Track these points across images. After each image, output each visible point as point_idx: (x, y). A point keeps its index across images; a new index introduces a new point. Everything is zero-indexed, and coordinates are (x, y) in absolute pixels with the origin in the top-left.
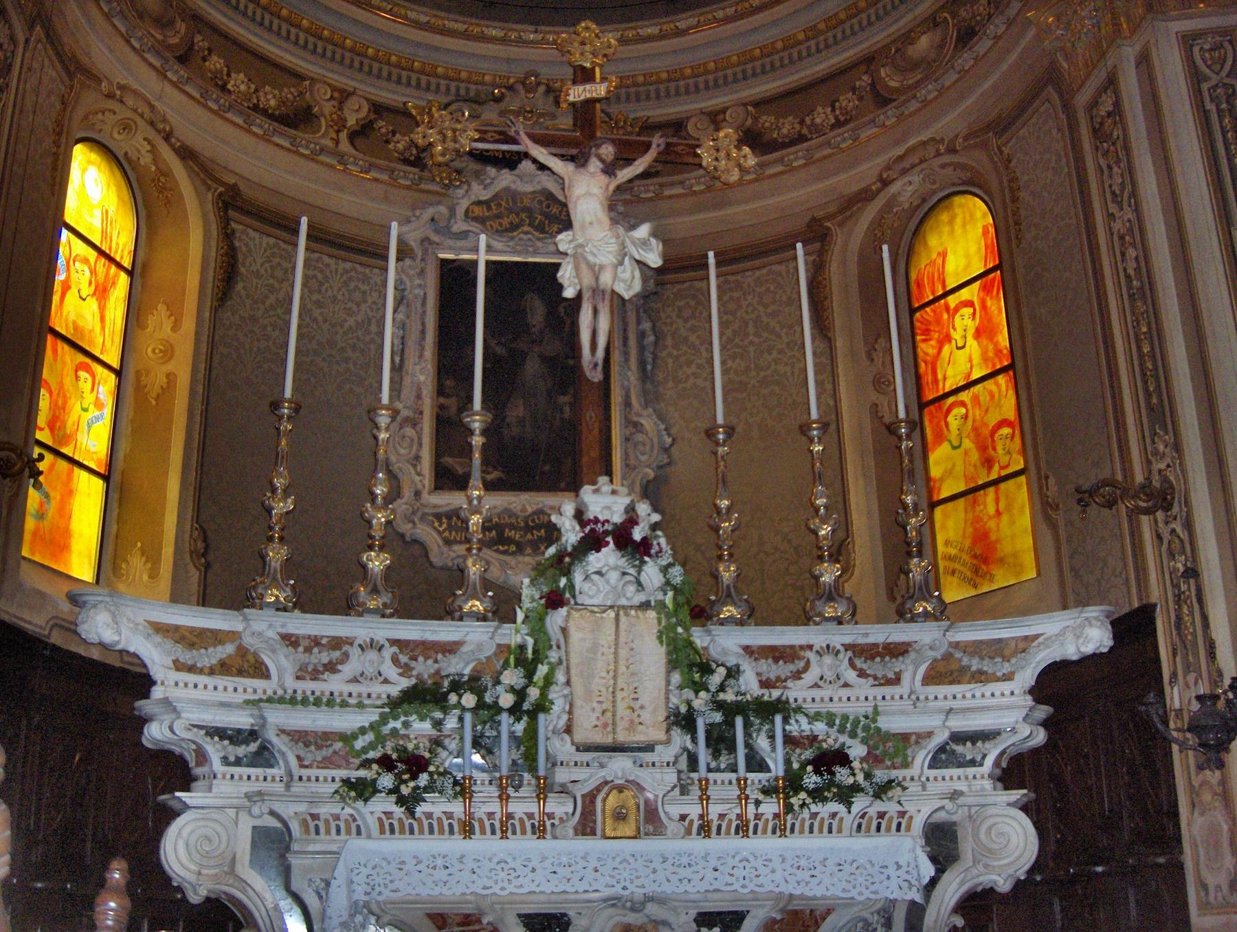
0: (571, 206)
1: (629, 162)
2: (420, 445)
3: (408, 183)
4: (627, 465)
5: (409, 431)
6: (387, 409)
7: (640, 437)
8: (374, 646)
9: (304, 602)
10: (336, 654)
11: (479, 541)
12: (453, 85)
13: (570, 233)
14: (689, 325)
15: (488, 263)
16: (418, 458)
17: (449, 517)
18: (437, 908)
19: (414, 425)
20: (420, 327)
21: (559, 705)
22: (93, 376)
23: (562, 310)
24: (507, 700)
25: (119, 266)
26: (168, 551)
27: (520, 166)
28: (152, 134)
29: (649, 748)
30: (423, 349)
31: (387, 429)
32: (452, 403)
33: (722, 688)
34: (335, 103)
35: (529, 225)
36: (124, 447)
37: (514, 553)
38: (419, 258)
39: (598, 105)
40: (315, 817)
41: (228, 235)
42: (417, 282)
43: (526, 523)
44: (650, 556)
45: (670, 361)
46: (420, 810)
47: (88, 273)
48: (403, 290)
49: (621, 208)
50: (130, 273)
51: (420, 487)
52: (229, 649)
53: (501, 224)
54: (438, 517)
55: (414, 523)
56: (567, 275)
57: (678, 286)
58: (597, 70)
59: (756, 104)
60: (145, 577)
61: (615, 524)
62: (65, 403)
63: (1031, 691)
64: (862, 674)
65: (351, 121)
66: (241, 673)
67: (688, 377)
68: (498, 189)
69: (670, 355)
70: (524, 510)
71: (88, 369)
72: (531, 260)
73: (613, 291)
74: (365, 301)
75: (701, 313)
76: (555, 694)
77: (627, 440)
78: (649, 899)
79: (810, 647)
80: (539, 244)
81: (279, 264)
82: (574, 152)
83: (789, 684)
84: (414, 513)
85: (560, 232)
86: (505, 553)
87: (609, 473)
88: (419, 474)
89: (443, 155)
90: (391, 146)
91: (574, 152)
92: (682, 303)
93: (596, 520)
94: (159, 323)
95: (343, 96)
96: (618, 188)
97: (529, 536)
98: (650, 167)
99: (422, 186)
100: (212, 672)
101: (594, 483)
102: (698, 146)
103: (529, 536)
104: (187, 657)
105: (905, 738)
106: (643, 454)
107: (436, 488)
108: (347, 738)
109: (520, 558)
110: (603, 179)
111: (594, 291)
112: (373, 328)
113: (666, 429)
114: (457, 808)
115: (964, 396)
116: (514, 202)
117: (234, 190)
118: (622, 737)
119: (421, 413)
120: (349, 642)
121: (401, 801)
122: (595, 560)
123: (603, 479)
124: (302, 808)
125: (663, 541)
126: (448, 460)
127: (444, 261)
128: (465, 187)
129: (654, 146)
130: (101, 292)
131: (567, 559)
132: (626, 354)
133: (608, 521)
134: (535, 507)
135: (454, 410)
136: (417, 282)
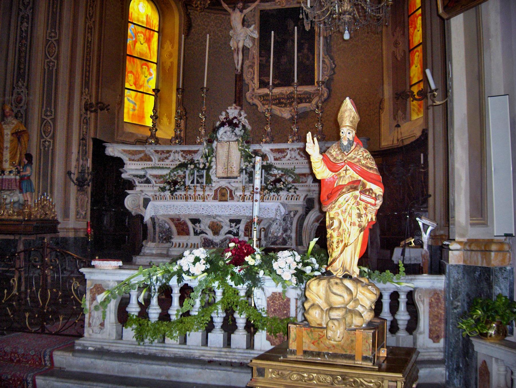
2: (254, 74)
8: (176, 152)
10: (168, 155)
16: (253, 78)
17: (263, 97)
18: (172, 217)
21: (214, 167)
22: (148, 67)
29: (236, 178)
32: (264, 59)
37: (284, 107)
40: (156, 195)
42: (252, 19)
45: (335, 38)
47: (143, 36)
52: (142, 155)
54: (260, 96)
60: (168, 124)
62: (139, 76)
66: (145, 160)
71: (146, 65)
78: (217, 216)
79: (288, 149)
83: (282, 159)
84: (253, 96)
86: (281, 107)
94: (168, 47)
97: (288, 101)
100: (138, 161)
104: (133, 157)
109: (286, 108)
118: (229, 175)
120: (171, 151)
124: (153, 193)
126: (262, 78)
130: (148, 40)
135: (264, 61)
136: (252, 19)
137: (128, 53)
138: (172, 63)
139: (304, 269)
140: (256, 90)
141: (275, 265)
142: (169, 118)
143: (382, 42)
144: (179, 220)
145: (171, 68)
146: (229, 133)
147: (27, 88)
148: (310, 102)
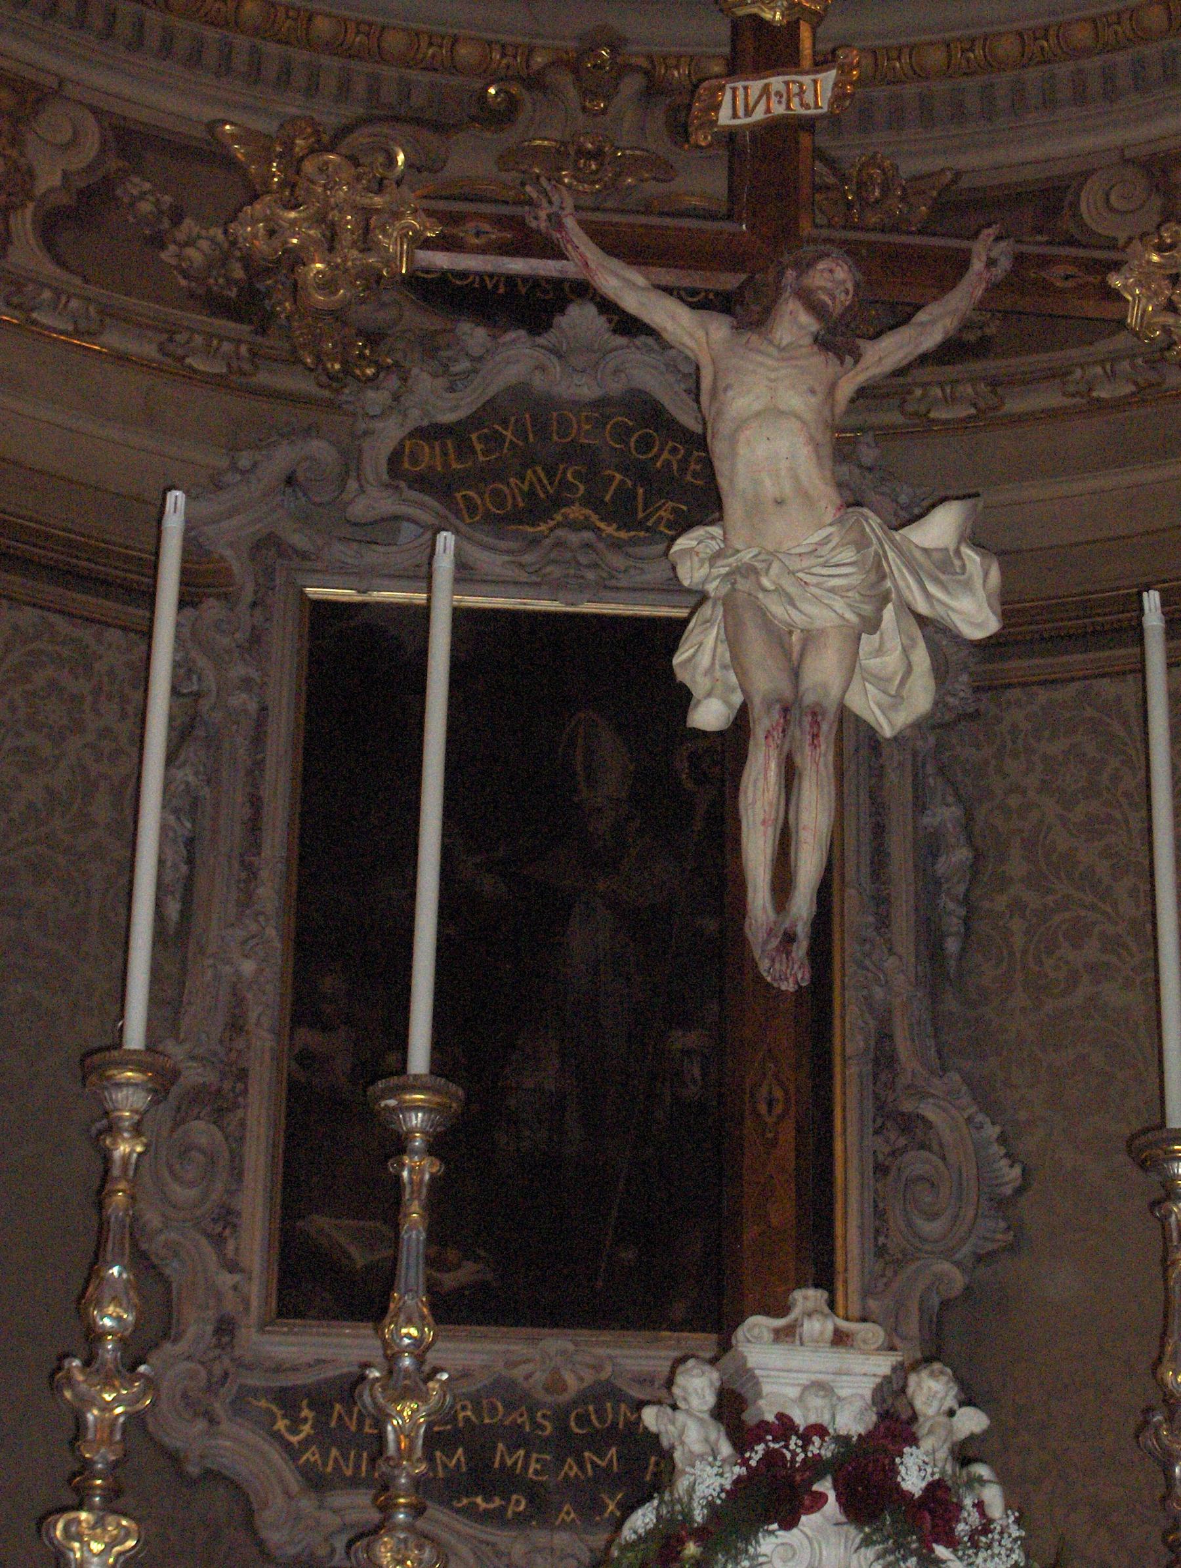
0: (718, 448)
1: (902, 317)
2: (237, 1173)
3: (220, 368)
4: (881, 1251)
5: (201, 1131)
6: (141, 1067)
7: (917, 1163)
11: (418, 1483)
12: (361, 69)
13: (716, 530)
14: (1079, 813)
15: (461, 616)
16: (227, 1217)
17: (321, 1406)
19: (219, 1115)
20: (247, 812)
23: (682, 766)
27: (561, 321)
30: (252, 873)
31: (137, 1130)
35: (586, 502)
37: (521, 1521)
38: (248, 596)
39: (805, 139)
42: (239, 670)
43: (563, 1429)
44: (952, 1542)
48: (197, 696)
49: (868, 455)
51: (231, 1305)
53: (499, 498)
54: (287, 1399)
55: (213, 1421)
56: (705, 660)
57: (1043, 696)
58: (805, 32)
61: (843, 1440)
65: (48, 178)
67: (1073, 979)
68: (491, 391)
69: (1017, 906)
70: (555, 1385)
72: (589, 608)
73: (843, 713)
74: (78, 727)
75: (1116, 778)
77: (881, 1170)
80: (617, 560)
81: (53, 685)
82: (729, 281)
85: (683, 525)
86: (496, 1518)
87: (825, 1278)
88: (233, 1267)
89: (328, 284)
90: (168, 255)
91: (729, 281)
92: (1056, 748)
93: (785, 1427)
96: (862, 393)
98: (966, 325)
99: (263, 378)
101: (781, 1310)
102: (1116, 266)
103: (571, 1469)
106: (933, 1216)
107: (280, 1314)
109: (541, 1537)
110: (820, 365)
111: (786, 710)
112: (102, 809)
113: (1003, 1139)
116: (542, 430)
119: (242, 1075)
123: (807, 1298)
125: (993, 1496)
127: (322, 607)
128: (393, 382)
129: (977, 265)
131: (692, 1549)
132: (881, 902)
133: (820, 1430)
134: (589, 1377)
136: (239, 670)
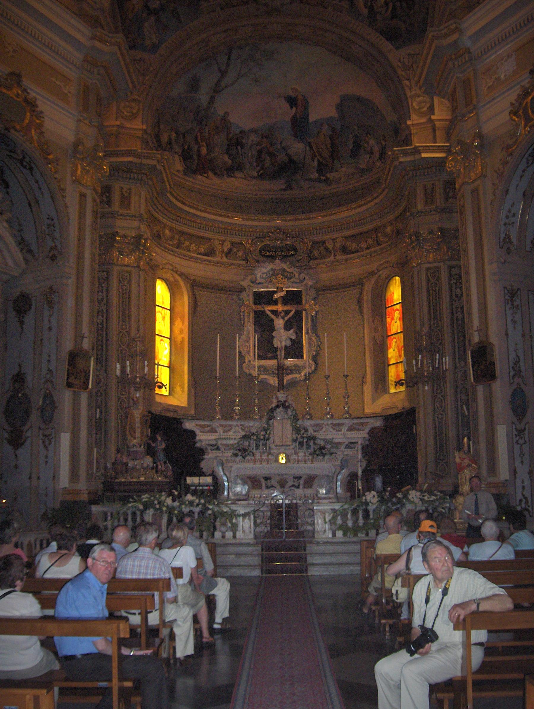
8: (237, 426)
9: (224, 418)
16: (249, 351)
24: (262, 437)
25: (167, 309)
26: (186, 385)
28: (172, 272)
29: (289, 446)
33: (303, 434)
34: (220, 245)
36: (173, 358)
41: (194, 294)
46: (246, 458)
50: (170, 310)
59: (346, 237)
63: (368, 433)
64: (334, 429)
65: (225, 250)
76: (271, 436)
94: (178, 323)
95: (222, 242)
100: (207, 432)
105: (339, 443)
108: (232, 445)
114: (253, 458)
115: (396, 336)
117: (195, 281)
118: (284, 444)
121: (243, 457)
122: (278, 410)
124: (225, 458)
137: (157, 333)
138: (183, 338)
139: (424, 498)
140: (252, 362)
141: (410, 497)
142: (182, 387)
143: (363, 328)
144: (255, 477)
145: (182, 343)
146: (282, 413)
147: (106, 371)
148: (300, 373)
